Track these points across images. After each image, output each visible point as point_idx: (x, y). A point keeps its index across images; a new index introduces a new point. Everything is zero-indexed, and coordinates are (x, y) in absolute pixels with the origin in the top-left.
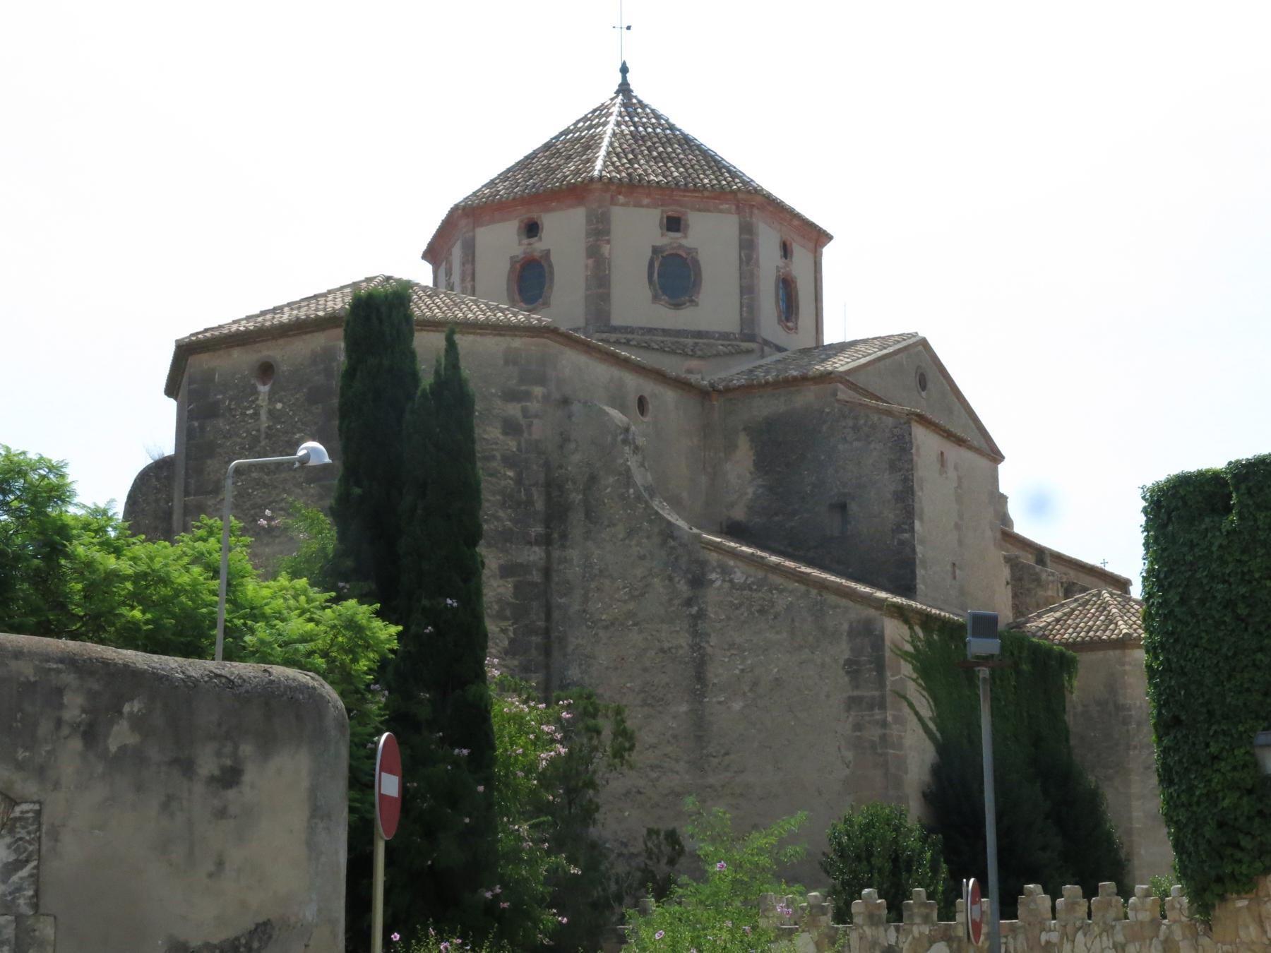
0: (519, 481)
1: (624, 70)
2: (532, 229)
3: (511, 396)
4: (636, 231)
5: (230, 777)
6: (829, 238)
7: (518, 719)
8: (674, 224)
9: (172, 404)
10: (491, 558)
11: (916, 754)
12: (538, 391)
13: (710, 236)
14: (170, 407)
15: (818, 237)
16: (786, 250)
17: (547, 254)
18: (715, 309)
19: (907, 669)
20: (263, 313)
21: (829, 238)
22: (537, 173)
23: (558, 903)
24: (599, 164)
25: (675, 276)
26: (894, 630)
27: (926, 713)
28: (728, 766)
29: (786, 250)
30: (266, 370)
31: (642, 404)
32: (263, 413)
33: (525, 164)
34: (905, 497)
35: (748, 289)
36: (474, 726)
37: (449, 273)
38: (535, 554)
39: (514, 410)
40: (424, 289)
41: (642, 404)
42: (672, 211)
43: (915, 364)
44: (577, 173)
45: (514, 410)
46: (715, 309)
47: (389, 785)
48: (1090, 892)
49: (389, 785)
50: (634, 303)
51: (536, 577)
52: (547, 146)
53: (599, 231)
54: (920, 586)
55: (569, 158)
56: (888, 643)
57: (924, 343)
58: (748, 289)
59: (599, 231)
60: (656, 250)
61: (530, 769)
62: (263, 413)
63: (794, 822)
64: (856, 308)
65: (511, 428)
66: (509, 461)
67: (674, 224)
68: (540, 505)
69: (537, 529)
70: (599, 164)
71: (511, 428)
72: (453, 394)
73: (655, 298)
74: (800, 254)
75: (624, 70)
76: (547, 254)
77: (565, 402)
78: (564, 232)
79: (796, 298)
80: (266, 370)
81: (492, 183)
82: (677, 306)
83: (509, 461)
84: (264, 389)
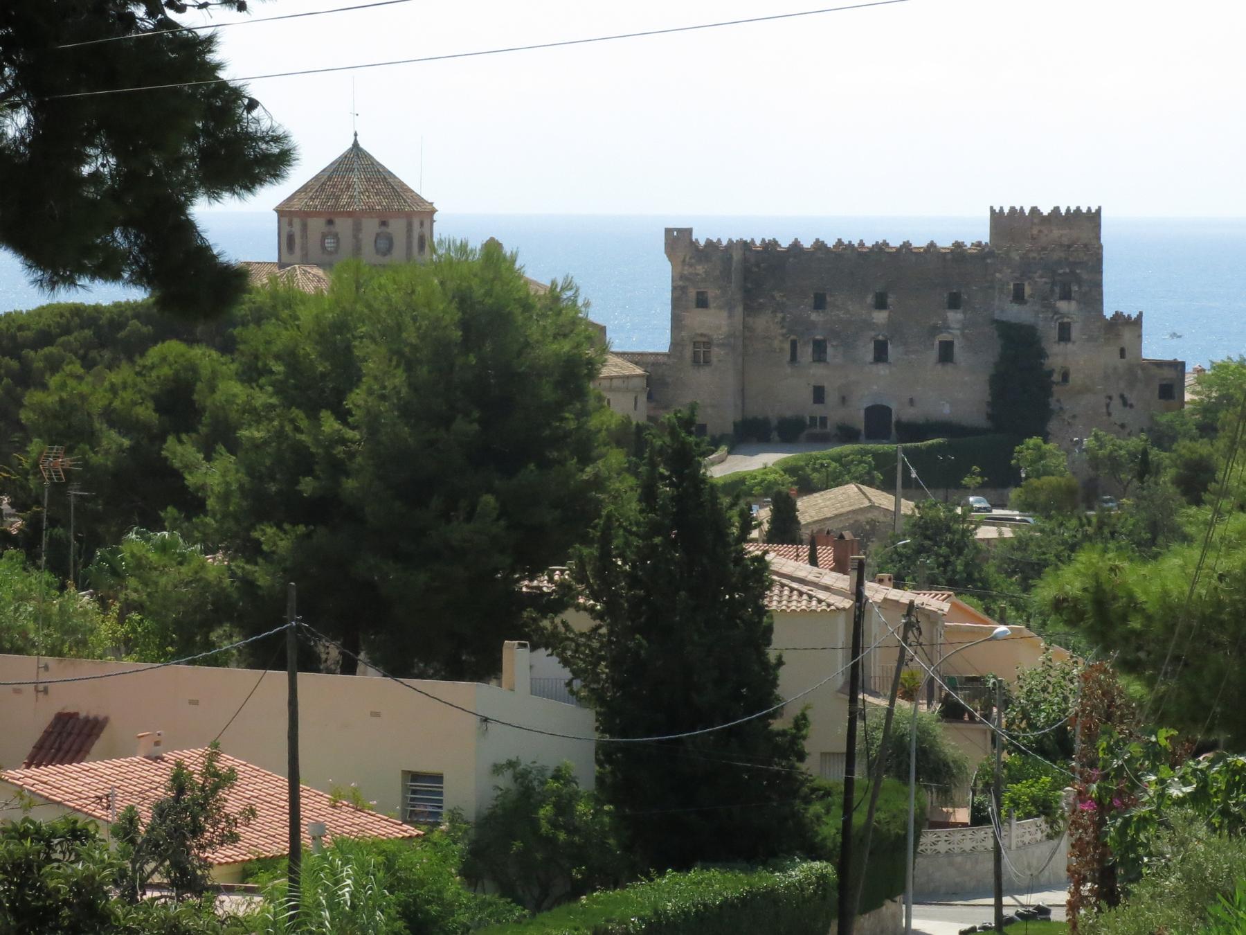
1: (356, 135)
8: (384, 224)
13: (397, 227)
16: (422, 224)
25: (385, 245)
29: (422, 224)
53: (357, 229)
67: (384, 224)
75: (356, 135)
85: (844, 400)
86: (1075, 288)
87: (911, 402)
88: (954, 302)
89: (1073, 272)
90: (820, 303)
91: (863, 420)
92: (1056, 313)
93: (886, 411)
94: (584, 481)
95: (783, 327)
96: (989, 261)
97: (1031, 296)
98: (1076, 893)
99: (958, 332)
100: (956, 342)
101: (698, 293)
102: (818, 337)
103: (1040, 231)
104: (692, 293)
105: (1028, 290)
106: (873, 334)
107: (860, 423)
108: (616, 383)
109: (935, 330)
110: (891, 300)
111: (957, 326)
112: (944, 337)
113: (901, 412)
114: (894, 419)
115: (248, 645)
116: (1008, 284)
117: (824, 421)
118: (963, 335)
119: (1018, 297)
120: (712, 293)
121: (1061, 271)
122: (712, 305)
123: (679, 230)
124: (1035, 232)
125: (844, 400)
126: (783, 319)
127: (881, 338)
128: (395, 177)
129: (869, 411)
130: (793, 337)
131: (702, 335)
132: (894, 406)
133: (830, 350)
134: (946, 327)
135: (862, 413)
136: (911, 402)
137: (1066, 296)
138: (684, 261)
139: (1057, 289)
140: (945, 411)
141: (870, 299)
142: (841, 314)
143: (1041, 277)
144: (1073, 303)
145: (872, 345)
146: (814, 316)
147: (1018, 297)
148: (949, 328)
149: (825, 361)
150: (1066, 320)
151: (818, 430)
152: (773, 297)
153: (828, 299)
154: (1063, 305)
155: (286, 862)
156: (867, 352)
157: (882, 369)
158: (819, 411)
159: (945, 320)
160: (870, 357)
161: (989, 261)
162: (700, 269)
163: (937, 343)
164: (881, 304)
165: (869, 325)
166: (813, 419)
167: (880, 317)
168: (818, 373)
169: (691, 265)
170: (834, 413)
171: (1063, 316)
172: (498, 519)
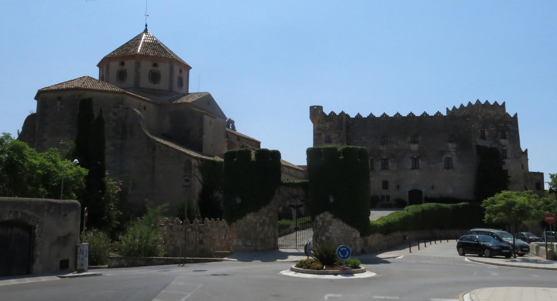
1: (146, 26)
2: (122, 64)
4: (146, 67)
5: (65, 215)
6: (191, 68)
7: (112, 185)
8: (155, 65)
9: (36, 102)
10: (108, 143)
11: (197, 186)
12: (121, 106)
13: (163, 68)
14: (36, 102)
15: (188, 68)
16: (181, 71)
17: (126, 70)
18: (163, 85)
19: (197, 170)
20: (59, 84)
21: (191, 68)
22: (124, 50)
23: (118, 219)
24: (139, 51)
25: (155, 77)
26: (194, 162)
27: (200, 178)
28: (189, 211)
29: (181, 71)
30: (59, 98)
31: (145, 108)
32: (58, 109)
33: (122, 47)
34: (201, 131)
36: (103, 186)
37: (103, 71)
39: (116, 110)
40: (97, 80)
41: (145, 108)
43: (207, 101)
44: (133, 52)
45: (116, 110)
46: (163, 85)
47: (86, 214)
48: (216, 220)
49: (86, 214)
50: (145, 82)
52: (127, 43)
53: (138, 65)
54: (204, 150)
55: (132, 48)
56: (193, 164)
57: (210, 95)
59: (138, 65)
60: (151, 71)
61: (113, 194)
62: (58, 109)
63: (165, 205)
64: (196, 85)
65: (115, 114)
67: (155, 65)
70: (139, 51)
71: (115, 114)
72: (100, 120)
73: (150, 81)
74: (184, 72)
75: (146, 26)
76: (126, 70)
77: (127, 108)
78: (130, 65)
79: (183, 82)
80: (59, 98)
81: (114, 52)
82: (155, 83)
84: (59, 102)
85: (398, 187)
86: (507, 133)
87: (433, 187)
91: (408, 197)
92: (500, 145)
93: (420, 192)
94: (168, 217)
96: (468, 119)
97: (488, 136)
100: (453, 158)
102: (384, 157)
103: (482, 111)
104: (323, 136)
105: (486, 133)
106: (411, 155)
107: (406, 198)
108: (292, 171)
109: (442, 153)
111: (454, 150)
112: (448, 155)
113: (426, 192)
114: (424, 196)
117: (388, 197)
119: (483, 137)
120: (333, 136)
121: (500, 125)
123: (317, 106)
124: (480, 110)
125: (398, 187)
127: (415, 157)
128: (174, 54)
129: (411, 192)
132: (423, 190)
133: (390, 163)
135: (407, 193)
136: (433, 187)
137: (504, 137)
138: (319, 122)
139: (500, 134)
140: (450, 192)
141: (409, 139)
143: (492, 127)
145: (411, 161)
146: (381, 148)
147: (483, 137)
148: (449, 151)
149: (388, 169)
150: (504, 148)
151: (385, 202)
154: (503, 141)
156: (409, 164)
157: (417, 172)
158: (385, 193)
160: (410, 166)
161: (468, 119)
162: (327, 125)
163: (443, 159)
166: (383, 197)
167: (415, 147)
168: (385, 175)
169: (322, 123)
170: (393, 193)
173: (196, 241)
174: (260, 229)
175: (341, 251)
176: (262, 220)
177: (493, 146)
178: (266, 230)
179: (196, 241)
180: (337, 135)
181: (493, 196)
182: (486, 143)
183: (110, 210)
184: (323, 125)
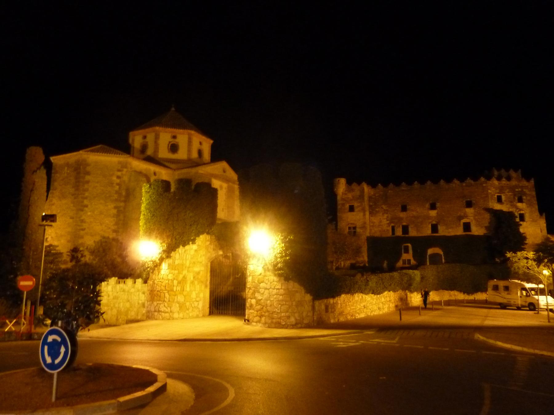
0: (120, 188)
3: (119, 171)
35: (189, 151)
38: (122, 204)
39: (119, 174)
42: (174, 134)
45: (119, 174)
51: (122, 209)
58: (189, 151)
60: (170, 142)
65: (118, 177)
66: (118, 184)
67: (174, 137)
68: (124, 193)
69: (123, 199)
71: (118, 177)
76: (147, 142)
83: (118, 184)
86: (524, 197)
88: (469, 205)
89: (522, 191)
90: (404, 209)
95: (387, 220)
97: (505, 201)
98: (97, 299)
99: (472, 218)
101: (350, 206)
102: (404, 224)
105: (503, 198)
106: (430, 221)
109: (460, 218)
110: (438, 205)
112: (465, 220)
115: (232, 310)
116: (494, 195)
118: (475, 219)
119: (499, 200)
120: (356, 204)
122: (356, 210)
126: (388, 217)
127: (434, 223)
130: (393, 225)
131: (351, 224)
133: (410, 229)
134: (466, 216)
137: (520, 200)
141: (428, 205)
142: (414, 213)
143: (508, 192)
144: (524, 204)
145: (430, 226)
147: (499, 200)
148: (467, 216)
150: (522, 212)
152: (382, 208)
153: (408, 207)
154: (519, 205)
155: (230, 184)
159: (465, 213)
163: (462, 224)
164: (433, 207)
165: (429, 217)
167: (433, 213)
171: (520, 210)
172: (514, 198)
173: (138, 303)
174: (179, 288)
175: (54, 358)
176: (181, 276)
177: (511, 210)
178: (188, 289)
179: (138, 303)
180: (359, 204)
181: (515, 253)
182: (504, 208)
183: (408, 287)
184: (346, 196)
